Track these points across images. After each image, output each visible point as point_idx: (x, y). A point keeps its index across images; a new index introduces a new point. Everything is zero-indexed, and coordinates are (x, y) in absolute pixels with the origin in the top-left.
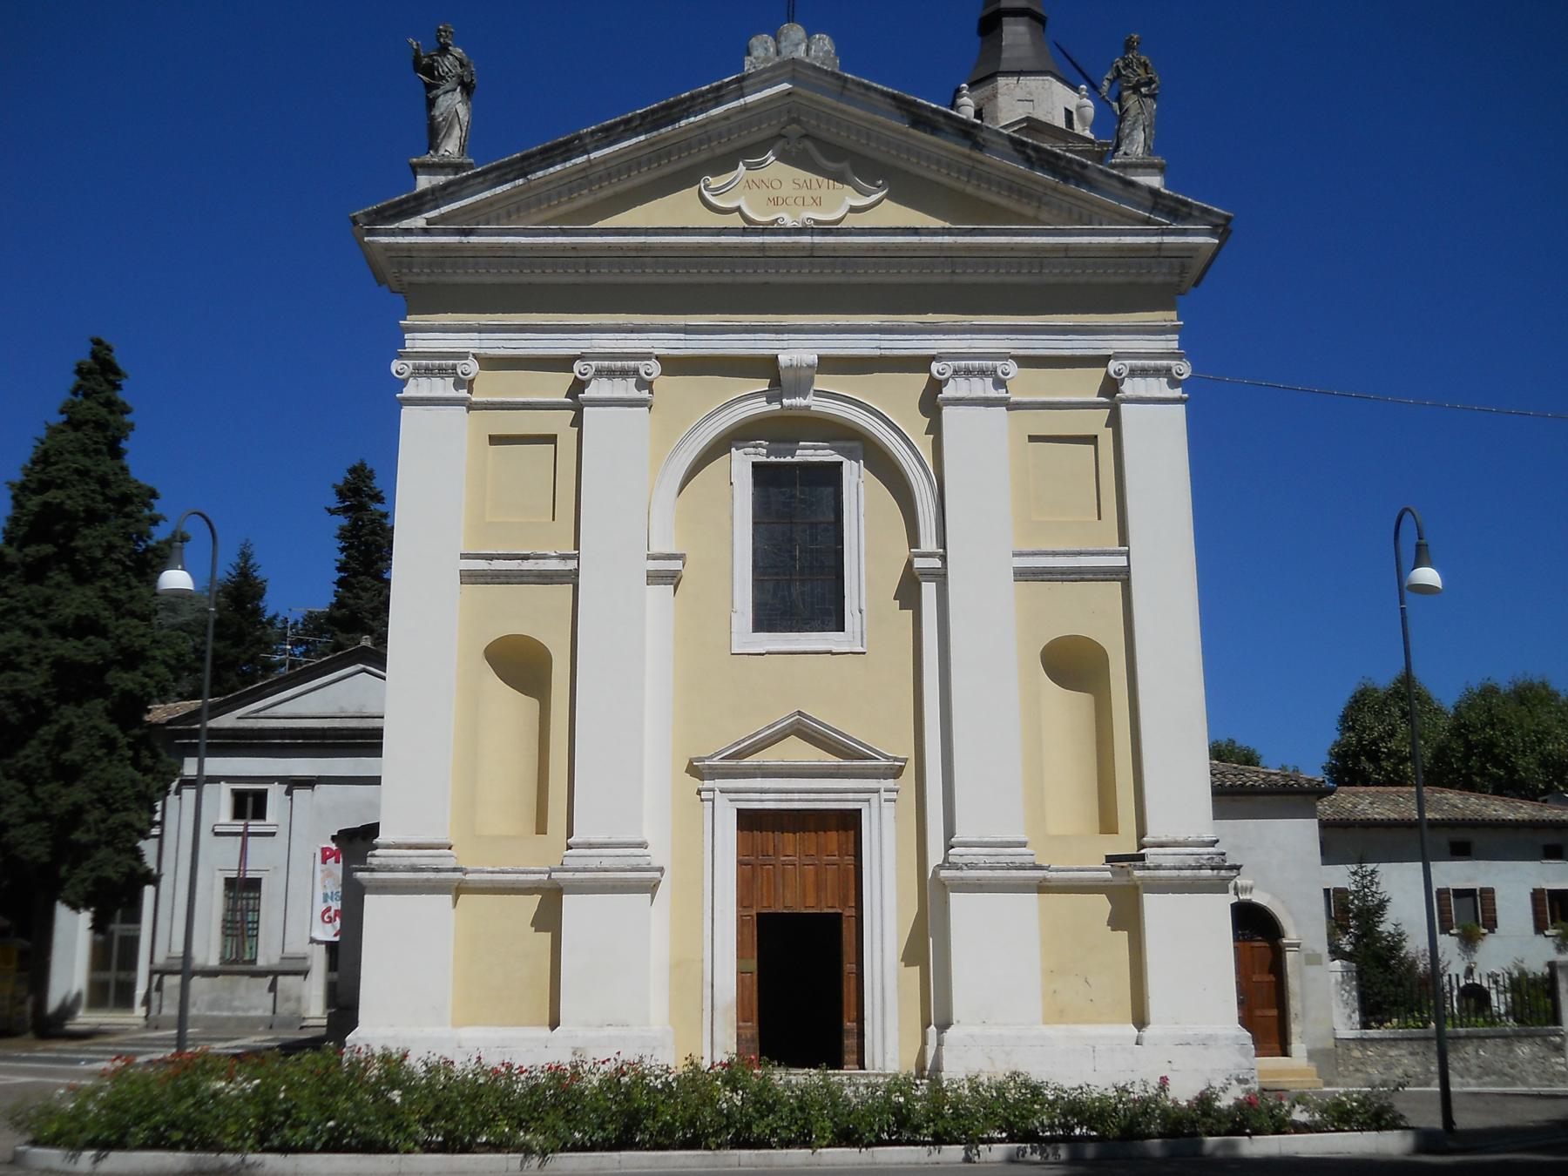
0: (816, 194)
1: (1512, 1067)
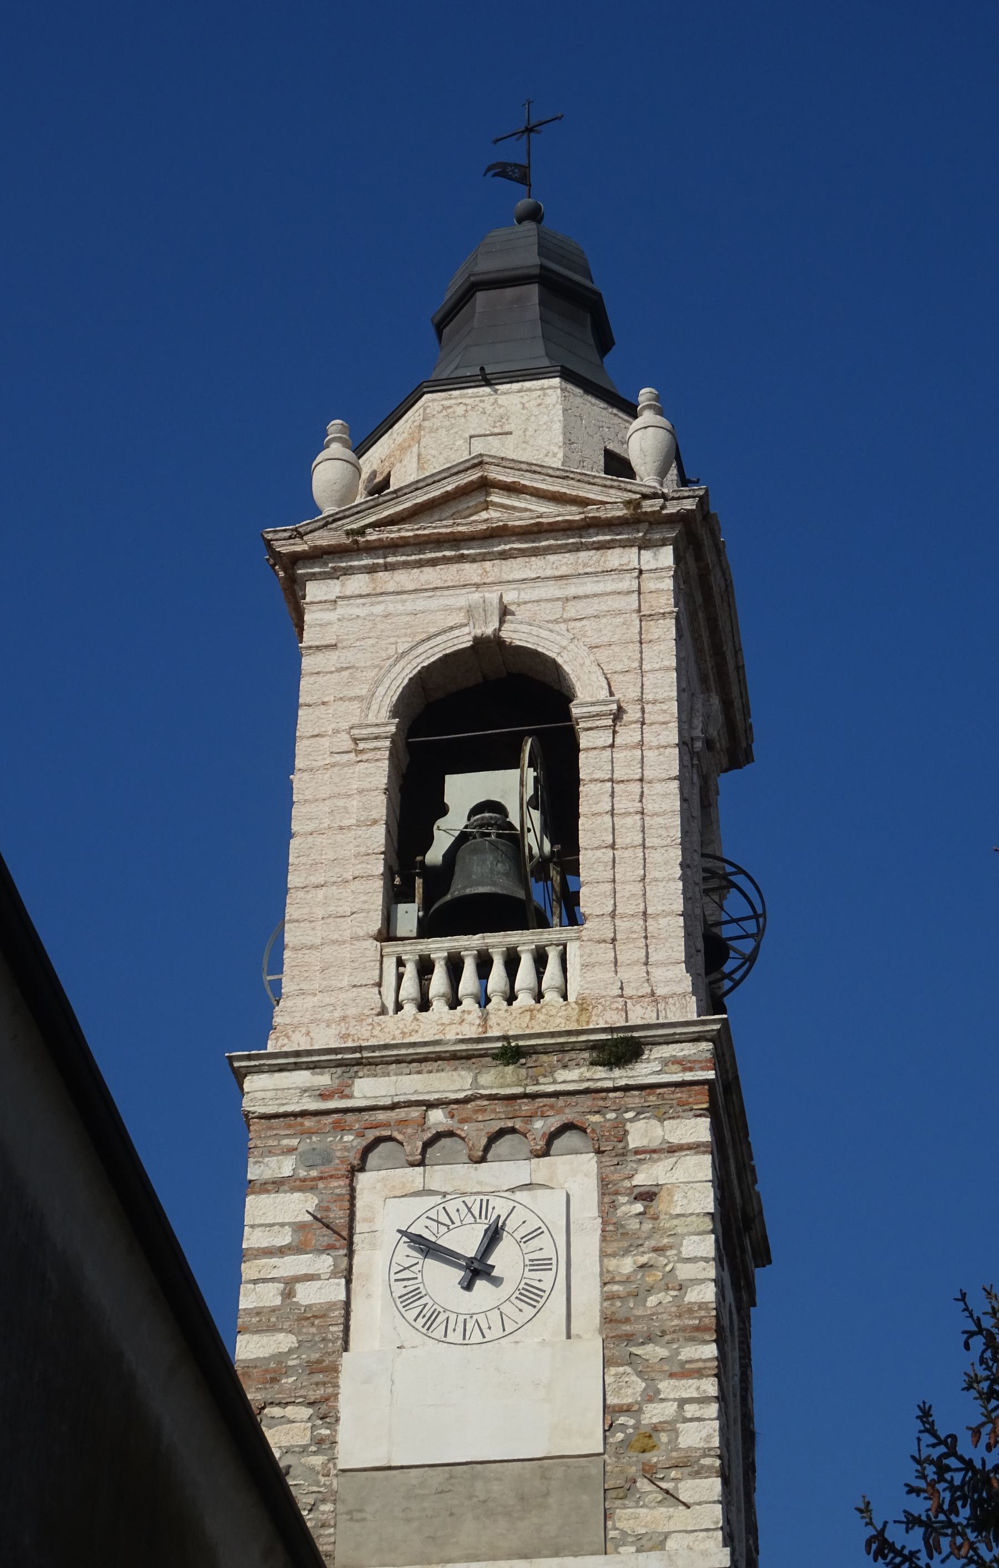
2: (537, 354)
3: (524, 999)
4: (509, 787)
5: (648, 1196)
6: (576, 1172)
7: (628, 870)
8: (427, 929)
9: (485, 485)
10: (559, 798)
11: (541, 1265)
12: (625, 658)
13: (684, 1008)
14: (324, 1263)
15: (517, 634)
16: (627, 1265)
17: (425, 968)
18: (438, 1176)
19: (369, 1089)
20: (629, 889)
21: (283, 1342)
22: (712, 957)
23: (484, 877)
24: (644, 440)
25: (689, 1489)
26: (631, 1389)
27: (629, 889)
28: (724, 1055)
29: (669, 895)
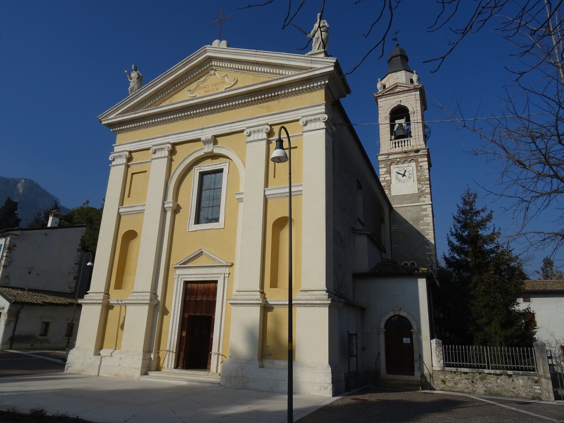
0: (217, 87)
1: (514, 388)
2: (402, 68)
3: (406, 146)
4: (402, 121)
5: (421, 166)
6: (413, 164)
7: (417, 131)
8: (395, 139)
9: (397, 86)
10: (408, 120)
11: (410, 174)
12: (414, 106)
13: (424, 146)
14: (388, 175)
15: (402, 104)
16: (419, 174)
17: (395, 143)
18: (399, 166)
19: (391, 157)
20: (417, 133)
21: (385, 184)
22: (425, 137)
23: (401, 133)
24: (415, 77)
25: (427, 196)
26: (421, 186)
27: (417, 133)
28: (428, 151)
29: (421, 133)
